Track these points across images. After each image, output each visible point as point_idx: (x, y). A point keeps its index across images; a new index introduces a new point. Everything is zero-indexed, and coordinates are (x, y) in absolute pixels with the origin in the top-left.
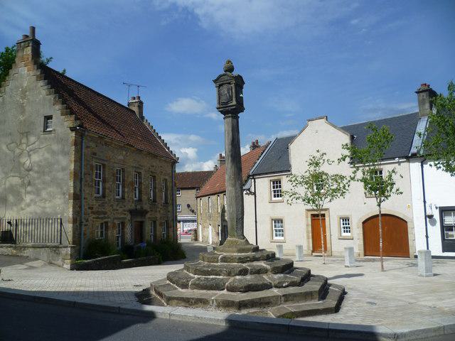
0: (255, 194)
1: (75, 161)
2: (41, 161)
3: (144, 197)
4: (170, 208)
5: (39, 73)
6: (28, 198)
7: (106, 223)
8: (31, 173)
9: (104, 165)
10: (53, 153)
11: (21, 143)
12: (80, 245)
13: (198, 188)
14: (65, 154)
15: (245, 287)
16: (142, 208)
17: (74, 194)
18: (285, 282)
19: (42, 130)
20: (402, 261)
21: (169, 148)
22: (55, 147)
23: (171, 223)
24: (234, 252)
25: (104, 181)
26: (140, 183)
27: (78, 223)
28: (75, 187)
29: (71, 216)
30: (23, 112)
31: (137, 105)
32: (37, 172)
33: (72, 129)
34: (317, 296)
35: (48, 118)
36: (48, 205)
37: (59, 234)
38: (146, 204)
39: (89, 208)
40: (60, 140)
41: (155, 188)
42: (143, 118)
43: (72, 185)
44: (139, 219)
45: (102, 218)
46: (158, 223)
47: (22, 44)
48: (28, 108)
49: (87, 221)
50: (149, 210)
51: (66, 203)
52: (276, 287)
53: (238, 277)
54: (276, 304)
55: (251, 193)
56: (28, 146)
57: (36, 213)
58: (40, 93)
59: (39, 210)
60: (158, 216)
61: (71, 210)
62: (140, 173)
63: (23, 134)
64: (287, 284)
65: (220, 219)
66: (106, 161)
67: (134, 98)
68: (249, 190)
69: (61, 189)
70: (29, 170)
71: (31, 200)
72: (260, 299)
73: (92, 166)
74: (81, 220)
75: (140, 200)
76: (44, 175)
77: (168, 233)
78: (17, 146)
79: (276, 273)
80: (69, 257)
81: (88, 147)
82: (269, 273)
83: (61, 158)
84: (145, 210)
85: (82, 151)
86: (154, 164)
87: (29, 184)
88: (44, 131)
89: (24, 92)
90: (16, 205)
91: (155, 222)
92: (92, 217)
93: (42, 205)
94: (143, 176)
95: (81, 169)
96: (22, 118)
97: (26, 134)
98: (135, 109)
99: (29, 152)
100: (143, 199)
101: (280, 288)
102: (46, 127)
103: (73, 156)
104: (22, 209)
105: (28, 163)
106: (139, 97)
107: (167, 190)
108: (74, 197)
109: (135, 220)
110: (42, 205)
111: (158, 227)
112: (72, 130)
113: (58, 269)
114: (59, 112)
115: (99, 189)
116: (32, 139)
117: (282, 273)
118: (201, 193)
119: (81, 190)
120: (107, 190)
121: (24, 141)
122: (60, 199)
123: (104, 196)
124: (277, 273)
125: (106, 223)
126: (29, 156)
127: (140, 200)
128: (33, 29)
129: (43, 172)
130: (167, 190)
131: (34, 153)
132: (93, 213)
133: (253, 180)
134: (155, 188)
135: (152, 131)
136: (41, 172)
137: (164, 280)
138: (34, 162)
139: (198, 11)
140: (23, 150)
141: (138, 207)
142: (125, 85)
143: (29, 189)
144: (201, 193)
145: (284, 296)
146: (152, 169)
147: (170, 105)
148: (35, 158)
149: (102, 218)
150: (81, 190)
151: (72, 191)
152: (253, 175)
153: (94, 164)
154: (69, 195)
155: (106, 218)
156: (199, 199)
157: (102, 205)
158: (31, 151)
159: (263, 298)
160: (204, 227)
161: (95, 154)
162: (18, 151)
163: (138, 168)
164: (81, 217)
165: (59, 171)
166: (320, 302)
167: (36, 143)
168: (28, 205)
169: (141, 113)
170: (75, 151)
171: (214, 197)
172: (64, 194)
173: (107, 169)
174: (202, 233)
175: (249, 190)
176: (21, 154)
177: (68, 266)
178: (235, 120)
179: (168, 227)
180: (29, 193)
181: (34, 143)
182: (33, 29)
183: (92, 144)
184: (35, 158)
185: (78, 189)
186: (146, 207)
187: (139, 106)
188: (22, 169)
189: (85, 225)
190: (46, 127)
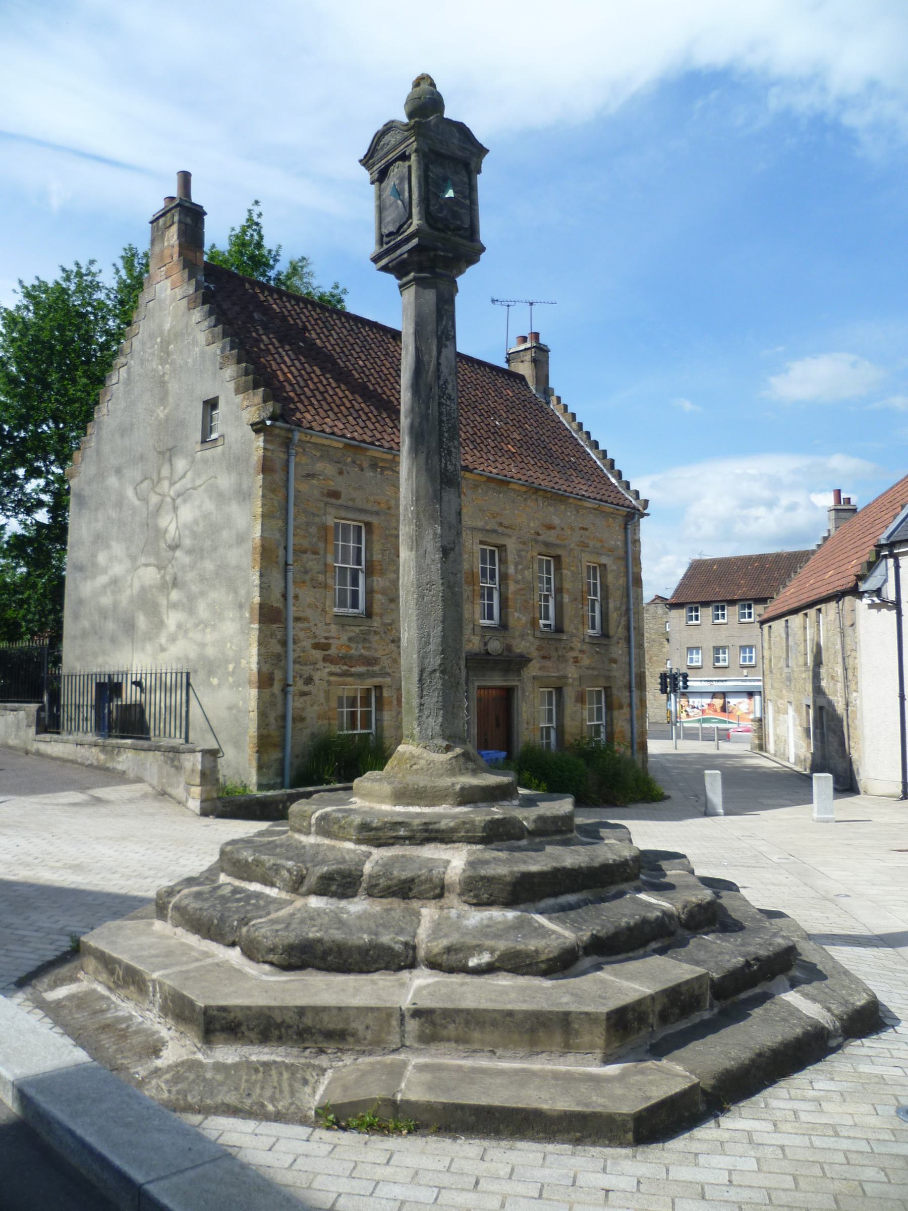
0: (897, 605)
1: (263, 516)
2: (196, 522)
3: (518, 619)
4: (618, 651)
5: (191, 290)
6: (172, 619)
7: (379, 688)
8: (178, 553)
9: (368, 525)
10: (220, 497)
11: (160, 480)
12: (283, 749)
13: (762, 600)
14: (243, 496)
15: (290, 949)
16: (509, 648)
17: (262, 606)
18: (479, 949)
19: (199, 438)
20: (322, 978)
21: (619, 475)
22: (225, 482)
23: (621, 695)
24: (382, 802)
25: (369, 573)
26: (504, 577)
27: (277, 688)
28: (264, 588)
29: (254, 667)
30: (163, 399)
31: (528, 357)
32: (190, 552)
33: (258, 427)
34: (598, 1036)
35: (211, 405)
36: (210, 637)
37: (184, 723)
38: (523, 636)
39: (316, 646)
40: (235, 463)
41: (559, 590)
42: (547, 392)
43: (257, 582)
44: (497, 680)
45: (360, 676)
46: (570, 694)
47: (161, 221)
48: (173, 387)
49: (309, 681)
50: (534, 654)
51: (244, 632)
52: (434, 965)
53: (315, 902)
54: (377, 1045)
55: (884, 604)
56: (172, 484)
57: (187, 659)
58: (195, 342)
59: (193, 652)
60: (572, 672)
61: (254, 650)
62: (502, 548)
63: (162, 453)
64: (486, 958)
65: (809, 687)
66: (377, 513)
67: (524, 339)
68: (878, 592)
69: (236, 592)
70: (174, 547)
71: (179, 626)
72: (301, 1011)
73: (324, 528)
74: (285, 679)
75: (504, 625)
76: (202, 558)
77: (610, 724)
78: (153, 488)
79: (479, 904)
80: (198, 780)
81: (310, 476)
82: (452, 899)
83: (234, 509)
84: (522, 656)
85: (287, 488)
86: (556, 521)
87: (175, 583)
88: (204, 441)
89: (165, 344)
90: (150, 639)
91: (559, 690)
92: (322, 673)
93: (198, 637)
94: (511, 556)
95: (286, 540)
96: (161, 413)
97: (168, 454)
98: (525, 369)
99: (174, 500)
100: (512, 622)
101: (451, 970)
102: (207, 429)
103: (259, 503)
104: (163, 649)
105: (172, 529)
106: (536, 336)
107: (605, 598)
108: (261, 614)
109: (477, 684)
110: (198, 637)
111: (570, 706)
112: (257, 431)
113: (178, 808)
114: (231, 386)
115: (490, 607)
116: (181, 464)
117: (509, 904)
118: (773, 608)
119: (285, 596)
120: (378, 597)
121: (165, 472)
122: (233, 620)
123: (369, 614)
124: (490, 903)
125: (379, 688)
126: (175, 509)
127: (504, 625)
128: (185, 178)
129: (202, 550)
130: (605, 598)
131: (185, 501)
132: (325, 659)
133: (891, 562)
134: (559, 590)
135: (572, 427)
136: (197, 552)
137: (211, 874)
138: (185, 525)
139: (851, 119)
140: (163, 496)
141: (495, 646)
142: (497, 306)
143: (175, 595)
144: (773, 608)
145: (418, 1013)
146: (550, 536)
147: (773, 380)
148: (187, 513)
149: (360, 676)
150: (285, 596)
151: (257, 600)
152: (892, 545)
153: (330, 521)
154: (251, 612)
155: (373, 675)
156: (766, 627)
157: (364, 638)
158: (179, 495)
159: (318, 1010)
160: (778, 711)
161: (335, 494)
162: (154, 499)
163: (494, 531)
164: (286, 672)
165: (231, 546)
166: (613, 1069)
167: (189, 475)
168: (173, 639)
169: (542, 377)
170: (264, 487)
171: (796, 620)
172: (241, 606)
173: (376, 537)
174: (775, 728)
175: (878, 592)
176: (159, 508)
177: (195, 805)
178: (430, 295)
179: (610, 707)
180: (174, 606)
181: (184, 476)
182: (185, 178)
183: (327, 468)
184: (187, 513)
185: (277, 592)
186: (521, 646)
187: (534, 361)
188: (163, 545)
189: (303, 694)
190: (207, 429)
